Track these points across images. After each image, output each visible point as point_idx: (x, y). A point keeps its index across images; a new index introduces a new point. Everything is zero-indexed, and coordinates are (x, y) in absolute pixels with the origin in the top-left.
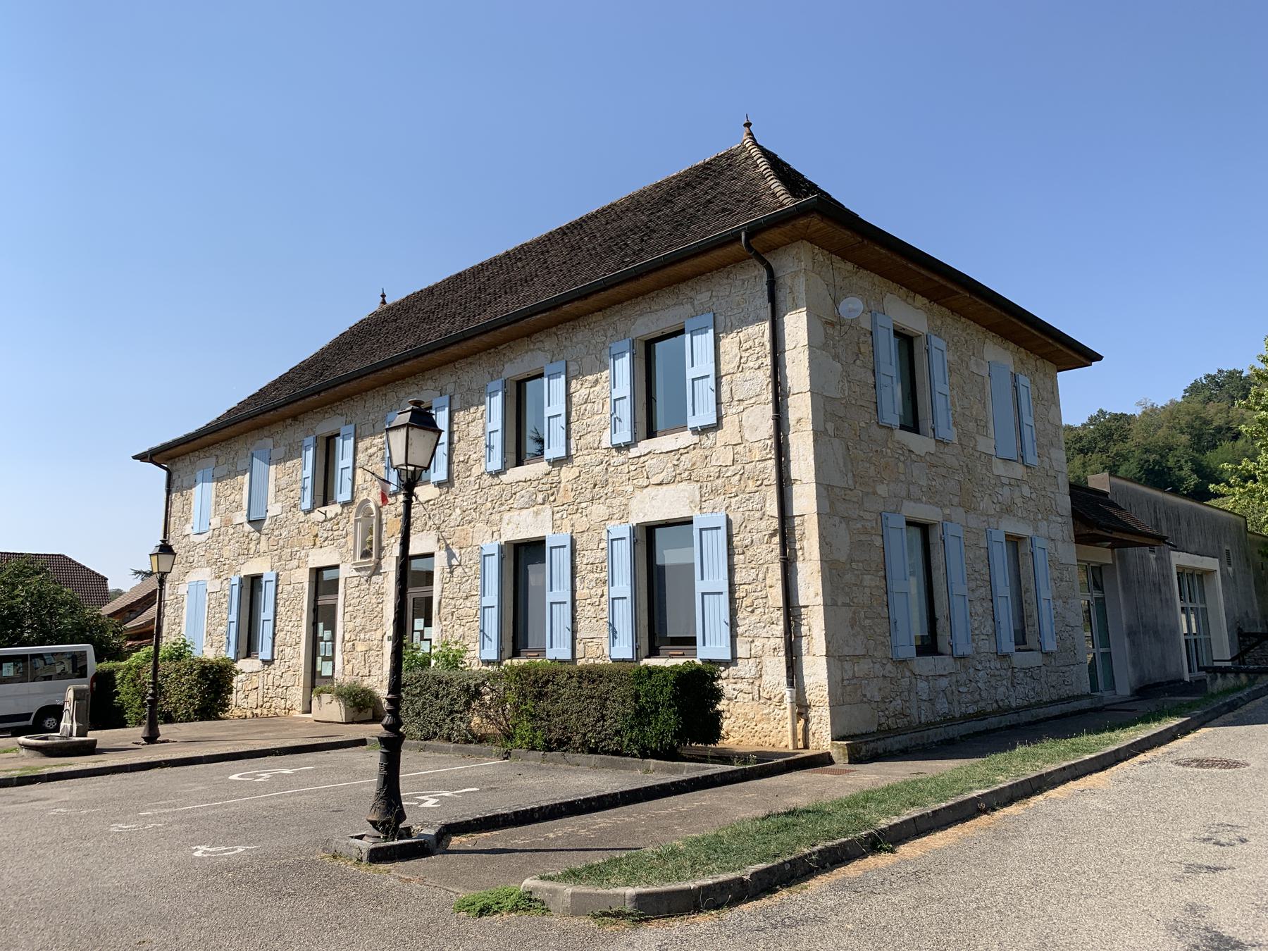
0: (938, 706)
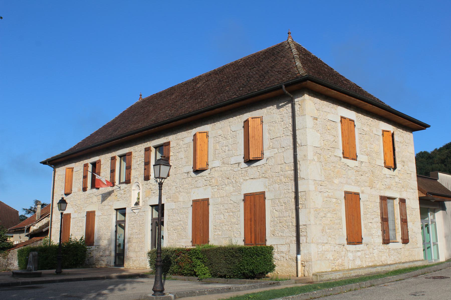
0: (357, 262)
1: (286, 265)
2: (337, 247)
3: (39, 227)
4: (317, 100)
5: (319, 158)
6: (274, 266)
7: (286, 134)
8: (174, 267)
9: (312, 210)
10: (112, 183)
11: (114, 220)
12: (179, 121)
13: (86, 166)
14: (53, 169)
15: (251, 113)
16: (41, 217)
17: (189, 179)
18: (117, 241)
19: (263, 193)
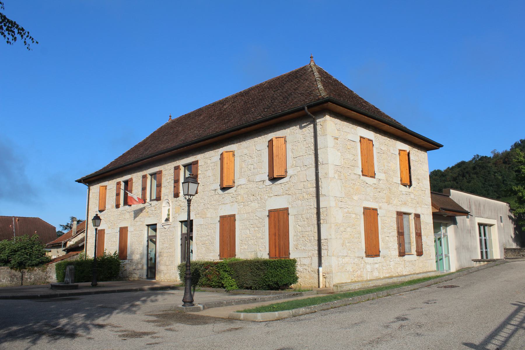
0: (375, 274)
1: (308, 277)
4: (337, 121)
5: (339, 176)
8: (203, 280)
10: (144, 201)
11: (146, 236)
12: (207, 141)
13: (118, 184)
15: (275, 133)
16: (77, 232)
18: (149, 255)
19: (287, 209)
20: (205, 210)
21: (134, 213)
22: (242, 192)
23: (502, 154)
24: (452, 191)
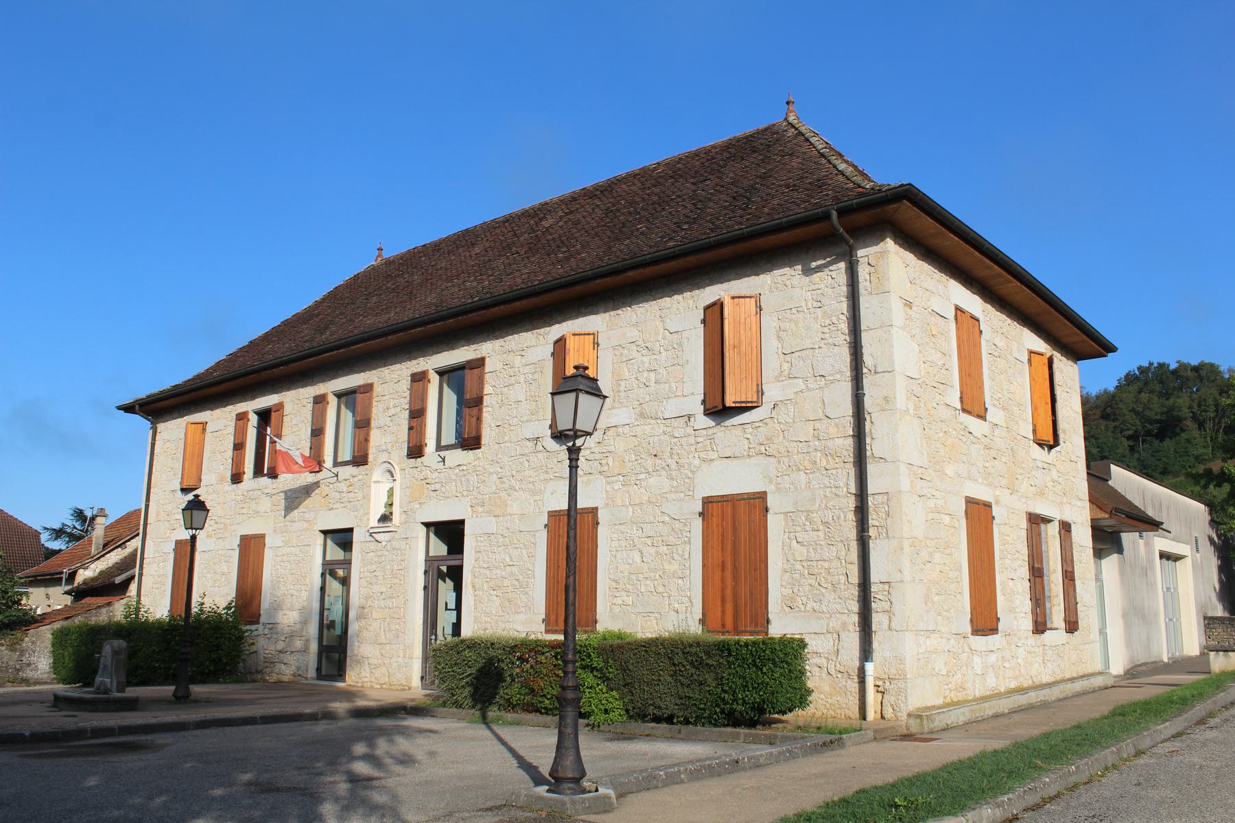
1: (827, 688)
2: (952, 641)
3: (98, 571)
4: (910, 257)
5: (917, 408)
6: (809, 692)
7: (830, 341)
8: (512, 691)
9: (906, 544)
10: (315, 461)
12: (518, 304)
13: (242, 417)
14: (148, 424)
15: (725, 286)
16: (105, 546)
17: (540, 456)
18: (326, 613)
19: (762, 496)
20: (503, 494)
21: (286, 499)
22: (619, 445)
23: (1097, 397)
24: (1115, 469)
